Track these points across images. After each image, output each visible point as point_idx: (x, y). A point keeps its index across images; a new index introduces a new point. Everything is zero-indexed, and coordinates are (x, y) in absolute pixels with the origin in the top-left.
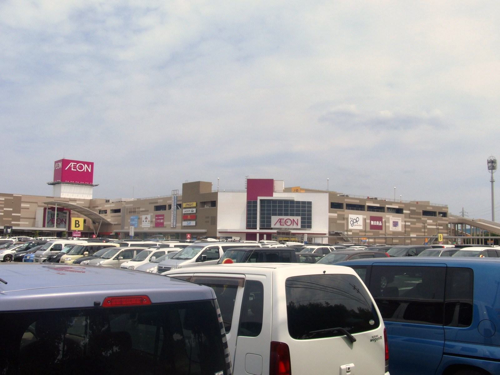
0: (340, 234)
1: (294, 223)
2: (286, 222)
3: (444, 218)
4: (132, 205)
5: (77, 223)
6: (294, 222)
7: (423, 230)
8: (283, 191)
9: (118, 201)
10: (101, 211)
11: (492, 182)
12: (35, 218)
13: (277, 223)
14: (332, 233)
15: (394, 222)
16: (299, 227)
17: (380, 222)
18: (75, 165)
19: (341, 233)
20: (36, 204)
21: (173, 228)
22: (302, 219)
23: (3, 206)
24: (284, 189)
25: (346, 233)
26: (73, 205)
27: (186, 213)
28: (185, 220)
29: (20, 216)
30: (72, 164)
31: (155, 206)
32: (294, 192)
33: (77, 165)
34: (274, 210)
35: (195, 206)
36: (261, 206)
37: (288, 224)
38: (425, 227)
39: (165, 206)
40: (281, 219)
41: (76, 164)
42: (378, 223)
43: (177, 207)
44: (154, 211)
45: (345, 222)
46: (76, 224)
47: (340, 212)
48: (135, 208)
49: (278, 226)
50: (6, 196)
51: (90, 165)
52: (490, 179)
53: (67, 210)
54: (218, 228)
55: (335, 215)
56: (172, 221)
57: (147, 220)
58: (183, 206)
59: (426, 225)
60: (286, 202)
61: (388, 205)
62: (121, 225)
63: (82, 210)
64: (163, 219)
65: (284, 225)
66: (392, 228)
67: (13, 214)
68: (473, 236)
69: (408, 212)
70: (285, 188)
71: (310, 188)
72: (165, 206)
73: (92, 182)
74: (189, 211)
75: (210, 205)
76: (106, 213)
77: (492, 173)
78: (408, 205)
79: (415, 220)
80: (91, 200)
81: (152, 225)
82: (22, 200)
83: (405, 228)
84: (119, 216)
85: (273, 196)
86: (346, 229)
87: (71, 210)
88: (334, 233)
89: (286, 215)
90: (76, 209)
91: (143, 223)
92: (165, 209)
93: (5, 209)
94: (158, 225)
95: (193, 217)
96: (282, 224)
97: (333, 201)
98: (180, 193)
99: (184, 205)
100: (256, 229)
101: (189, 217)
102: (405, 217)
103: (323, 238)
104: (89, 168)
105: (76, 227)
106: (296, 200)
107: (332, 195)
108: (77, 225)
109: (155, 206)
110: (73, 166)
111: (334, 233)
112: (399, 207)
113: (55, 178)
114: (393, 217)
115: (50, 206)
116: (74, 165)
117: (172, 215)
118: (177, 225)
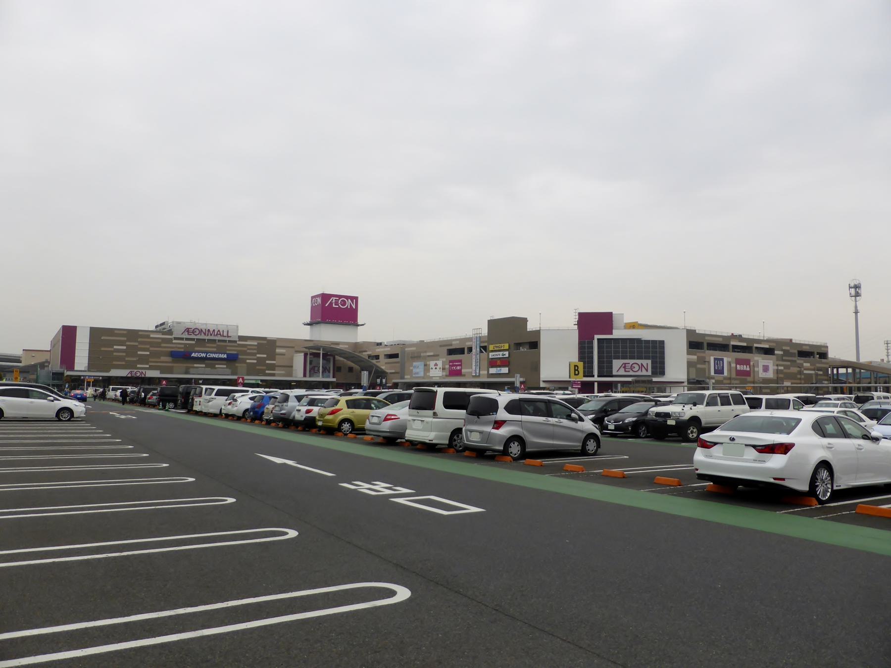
1: (643, 369)
2: (632, 368)
3: (823, 360)
7: (799, 376)
10: (371, 356)
11: (856, 312)
12: (292, 367)
13: (620, 369)
15: (763, 366)
16: (649, 373)
17: (748, 366)
19: (704, 381)
21: (475, 376)
27: (493, 357)
28: (492, 367)
29: (274, 364)
31: (447, 349)
33: (338, 300)
34: (616, 352)
35: (508, 348)
37: (195, 333)
38: (800, 373)
40: (625, 364)
41: (338, 298)
42: (745, 368)
43: (480, 349)
44: (447, 355)
46: (575, 370)
47: (700, 353)
49: (622, 372)
50: (258, 340)
52: (853, 309)
53: (330, 355)
55: (694, 357)
56: (474, 367)
57: (437, 367)
58: (489, 348)
59: (802, 369)
60: (632, 341)
62: (401, 373)
64: (460, 365)
66: (762, 375)
67: (267, 362)
68: (876, 383)
69: (781, 353)
71: (649, 323)
74: (500, 355)
75: (528, 347)
76: (379, 359)
77: (856, 301)
78: (781, 343)
79: (789, 363)
81: (444, 374)
82: (278, 344)
83: (777, 373)
84: (398, 362)
86: (707, 375)
87: (336, 356)
88: (695, 381)
89: (632, 358)
91: (431, 370)
92: (464, 353)
93: (258, 355)
94: (453, 373)
95: (504, 363)
97: (692, 340)
98: (485, 332)
99: (491, 347)
100: (593, 376)
101: (499, 363)
102: (777, 360)
105: (575, 374)
107: (690, 333)
108: (577, 372)
109: (447, 349)
112: (769, 346)
114: (763, 359)
116: (335, 300)
117: (474, 360)
118: (481, 372)
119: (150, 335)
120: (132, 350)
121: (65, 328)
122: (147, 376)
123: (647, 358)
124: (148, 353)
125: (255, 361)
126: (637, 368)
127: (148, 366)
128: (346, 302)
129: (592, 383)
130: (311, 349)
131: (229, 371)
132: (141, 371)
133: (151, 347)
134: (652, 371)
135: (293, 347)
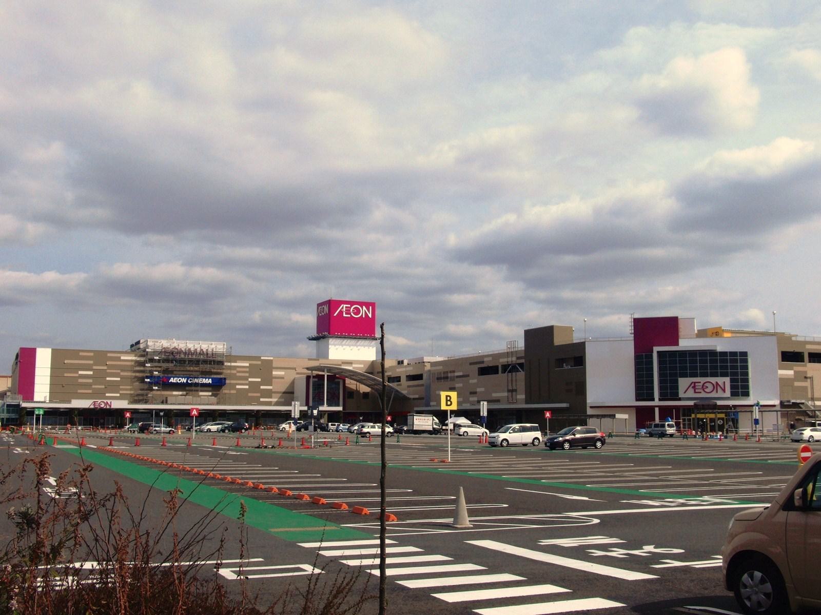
0: (801, 406)
4: (441, 367)
5: (448, 399)
6: (718, 387)
8: (695, 336)
9: (417, 362)
10: (391, 378)
12: (293, 393)
14: (785, 404)
16: (728, 393)
18: (348, 307)
19: (803, 403)
20: (294, 371)
22: (732, 381)
23: (247, 375)
24: (696, 332)
25: (810, 403)
26: (350, 371)
29: (271, 389)
30: (344, 307)
31: (479, 368)
32: (712, 336)
33: (350, 308)
36: (660, 363)
37: (706, 390)
39: (497, 367)
40: (695, 383)
41: (349, 306)
45: (807, 384)
46: (447, 401)
47: (798, 367)
48: (447, 372)
49: (690, 393)
51: (371, 307)
54: (589, 401)
61: (502, 359)
63: (363, 378)
65: (700, 392)
67: (262, 387)
70: (698, 331)
72: (497, 367)
73: (374, 334)
76: (400, 381)
80: (373, 361)
82: (274, 365)
84: (422, 385)
85: (680, 345)
87: (346, 379)
88: (791, 404)
90: (353, 377)
92: (497, 373)
93: (250, 380)
96: (697, 391)
98: (521, 345)
100: (653, 400)
103: (763, 413)
104: (369, 312)
105: (447, 405)
106: (719, 349)
107: (781, 337)
108: (449, 403)
109: (479, 368)
110: (346, 310)
111: (791, 404)
113: (319, 331)
115: (315, 373)
116: (346, 307)
119: (120, 357)
120: (99, 377)
121: (23, 350)
122: (113, 407)
123: (724, 375)
124: (119, 379)
125: (247, 387)
126: (710, 388)
127: (118, 395)
128: (358, 308)
129: (652, 408)
130: (314, 370)
131: (214, 399)
132: (105, 401)
133: (122, 371)
134: (731, 392)
135: (295, 369)
